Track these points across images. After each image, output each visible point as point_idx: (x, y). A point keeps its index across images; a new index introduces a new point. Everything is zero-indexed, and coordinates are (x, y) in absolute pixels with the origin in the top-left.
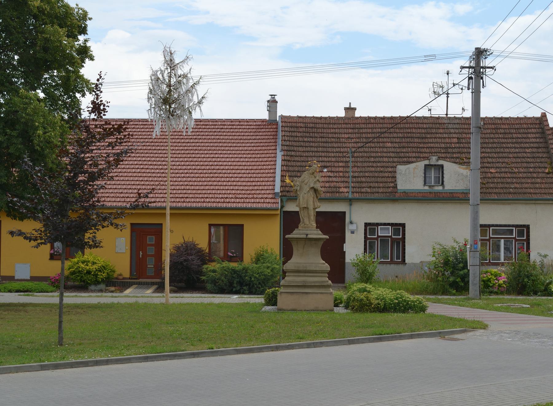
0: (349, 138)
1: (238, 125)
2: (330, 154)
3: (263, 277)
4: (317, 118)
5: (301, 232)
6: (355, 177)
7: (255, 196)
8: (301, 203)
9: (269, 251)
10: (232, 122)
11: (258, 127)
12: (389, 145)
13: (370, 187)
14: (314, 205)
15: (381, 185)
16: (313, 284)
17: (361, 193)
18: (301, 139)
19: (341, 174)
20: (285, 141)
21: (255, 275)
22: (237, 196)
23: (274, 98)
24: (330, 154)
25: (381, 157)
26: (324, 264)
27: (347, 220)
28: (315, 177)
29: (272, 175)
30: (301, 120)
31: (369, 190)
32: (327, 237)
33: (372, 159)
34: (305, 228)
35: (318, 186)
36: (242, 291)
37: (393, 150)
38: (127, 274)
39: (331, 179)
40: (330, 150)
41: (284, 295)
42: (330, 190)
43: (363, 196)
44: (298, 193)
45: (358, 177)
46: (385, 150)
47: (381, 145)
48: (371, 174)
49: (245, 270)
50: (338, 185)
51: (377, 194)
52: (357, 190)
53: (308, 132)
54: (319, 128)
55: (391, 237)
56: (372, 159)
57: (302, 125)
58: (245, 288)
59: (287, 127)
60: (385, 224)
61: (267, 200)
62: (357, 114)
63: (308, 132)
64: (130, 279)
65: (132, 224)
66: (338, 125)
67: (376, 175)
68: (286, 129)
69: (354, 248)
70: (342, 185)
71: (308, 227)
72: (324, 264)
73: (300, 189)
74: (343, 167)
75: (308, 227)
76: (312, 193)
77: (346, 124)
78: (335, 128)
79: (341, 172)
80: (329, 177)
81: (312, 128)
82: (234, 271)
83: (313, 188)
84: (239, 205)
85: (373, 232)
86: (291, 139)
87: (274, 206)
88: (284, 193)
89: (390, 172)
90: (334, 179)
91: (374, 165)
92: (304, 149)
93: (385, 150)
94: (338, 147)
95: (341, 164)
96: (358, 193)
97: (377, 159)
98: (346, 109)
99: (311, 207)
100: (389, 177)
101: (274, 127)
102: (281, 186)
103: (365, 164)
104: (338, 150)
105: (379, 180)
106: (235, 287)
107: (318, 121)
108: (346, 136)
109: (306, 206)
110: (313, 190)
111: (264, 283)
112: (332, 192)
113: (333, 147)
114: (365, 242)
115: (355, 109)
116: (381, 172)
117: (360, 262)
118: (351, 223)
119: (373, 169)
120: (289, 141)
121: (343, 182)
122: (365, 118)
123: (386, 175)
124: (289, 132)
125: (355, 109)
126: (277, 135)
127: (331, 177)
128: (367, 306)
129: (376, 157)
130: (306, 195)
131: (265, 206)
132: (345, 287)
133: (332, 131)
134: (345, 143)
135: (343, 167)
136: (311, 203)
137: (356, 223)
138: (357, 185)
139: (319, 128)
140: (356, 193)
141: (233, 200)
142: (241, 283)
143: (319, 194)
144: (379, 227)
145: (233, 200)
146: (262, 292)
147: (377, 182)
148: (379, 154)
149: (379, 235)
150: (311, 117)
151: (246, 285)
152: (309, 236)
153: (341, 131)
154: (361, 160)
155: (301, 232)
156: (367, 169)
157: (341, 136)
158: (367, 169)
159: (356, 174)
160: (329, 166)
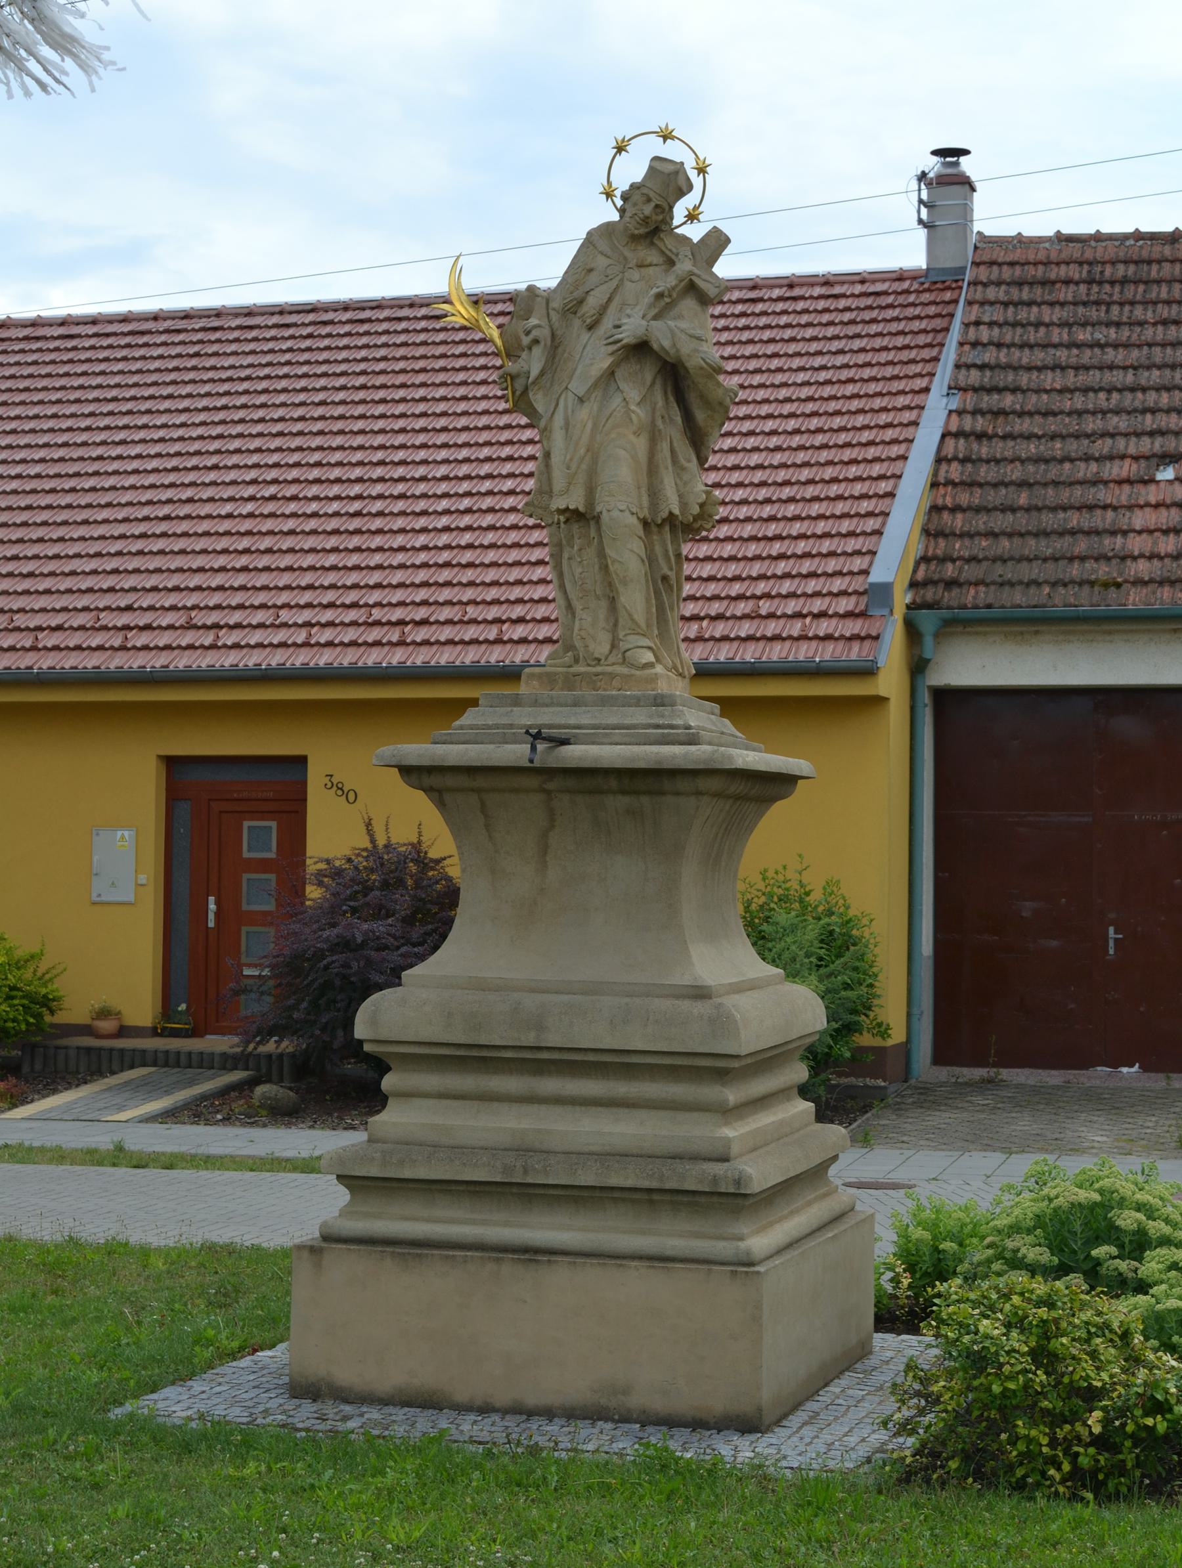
4: (1153, 237)
11: (869, 301)
16: (586, 1177)
18: (1056, 335)
20: (975, 344)
23: (957, 164)
28: (671, 263)
30: (1074, 251)
34: (570, 682)
38: (141, 1007)
53: (1097, 303)
54: (1158, 282)
57: (1074, 272)
59: (998, 284)
63: (1097, 303)
64: (154, 1032)
65: (172, 763)
68: (991, 293)
71: (592, 680)
75: (592, 680)
76: (636, 395)
81: (1124, 281)
83: (641, 349)
86: (1008, 339)
88: (930, 594)
92: (1071, 379)
107: (1157, 251)
109: (575, 501)
120: (999, 345)
124: (1006, 304)
128: (1036, 1415)
130: (584, 413)
131: (803, 652)
139: (1158, 282)
150: (1125, 237)
152: (576, 754)
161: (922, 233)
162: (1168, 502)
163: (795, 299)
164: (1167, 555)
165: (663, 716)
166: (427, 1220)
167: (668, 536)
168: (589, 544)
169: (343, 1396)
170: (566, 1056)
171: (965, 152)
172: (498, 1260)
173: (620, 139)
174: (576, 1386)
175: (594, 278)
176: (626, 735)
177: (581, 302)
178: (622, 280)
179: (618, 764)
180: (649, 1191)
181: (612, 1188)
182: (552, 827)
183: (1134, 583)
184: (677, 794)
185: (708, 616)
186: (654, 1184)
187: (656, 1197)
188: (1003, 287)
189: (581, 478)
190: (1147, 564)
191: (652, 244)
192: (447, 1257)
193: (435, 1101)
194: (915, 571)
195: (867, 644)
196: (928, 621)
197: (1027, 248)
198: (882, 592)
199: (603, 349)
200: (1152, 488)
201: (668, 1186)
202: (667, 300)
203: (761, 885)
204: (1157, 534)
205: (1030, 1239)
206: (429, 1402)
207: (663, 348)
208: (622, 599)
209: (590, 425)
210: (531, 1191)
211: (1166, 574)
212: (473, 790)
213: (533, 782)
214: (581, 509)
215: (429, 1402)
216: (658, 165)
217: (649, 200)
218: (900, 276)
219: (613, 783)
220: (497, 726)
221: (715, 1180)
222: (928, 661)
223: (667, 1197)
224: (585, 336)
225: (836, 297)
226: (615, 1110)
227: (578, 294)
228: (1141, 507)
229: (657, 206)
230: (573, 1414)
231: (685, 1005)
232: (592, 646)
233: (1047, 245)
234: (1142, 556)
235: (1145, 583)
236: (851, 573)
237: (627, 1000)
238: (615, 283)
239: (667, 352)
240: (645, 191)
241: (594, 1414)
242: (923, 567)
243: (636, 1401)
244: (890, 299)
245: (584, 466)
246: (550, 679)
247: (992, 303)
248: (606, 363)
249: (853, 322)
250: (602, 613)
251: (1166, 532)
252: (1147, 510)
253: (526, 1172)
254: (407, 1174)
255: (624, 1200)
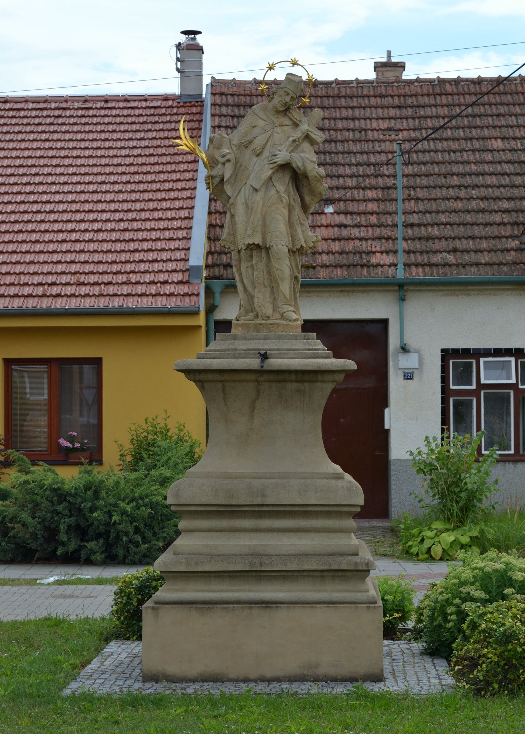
0: (389, 129)
1: (101, 108)
2: (341, 170)
3: (145, 511)
5: (240, 345)
6: (412, 225)
7: (133, 278)
8: (240, 228)
9: (173, 432)
10: (86, 101)
11: (152, 111)
12: (499, 144)
13: (455, 250)
14: (293, 237)
15: (484, 244)
17: (431, 265)
19: (373, 219)
21: (122, 504)
22: (82, 278)
23: (194, 39)
24: (341, 170)
25: (477, 174)
26: (339, 477)
27: (393, 342)
28: (296, 125)
29: (185, 224)
31: (451, 258)
32: (351, 365)
33: (455, 180)
34: (257, 328)
35: (307, 159)
36: (83, 554)
37: (509, 156)
39: (345, 232)
40: (340, 158)
41: (168, 616)
42: (343, 259)
43: (436, 275)
44: (228, 189)
45: (419, 225)
46: (488, 157)
47: (477, 144)
48: (454, 218)
49: (94, 489)
50: (365, 246)
51: (474, 269)
52: (420, 258)
55: (514, 387)
56: (455, 180)
58: (91, 545)
59: (227, 105)
60: (498, 352)
61: (168, 289)
62: (408, 75)
66: (360, 100)
67: (469, 218)
68: (224, 110)
69: (412, 423)
70: (376, 246)
71: (269, 327)
72: (339, 477)
73: (235, 174)
74: (377, 200)
76: (283, 186)
77: (381, 96)
78: (353, 108)
79: (372, 214)
80: (341, 226)
82: (60, 494)
84: (88, 303)
85: (464, 374)
87: (187, 303)
88: (216, 271)
89: (507, 211)
90: (355, 232)
91: (462, 193)
93: (488, 157)
94: (362, 153)
95: (371, 194)
96: (423, 266)
97: (468, 180)
98: (378, 67)
99: (281, 244)
100: (505, 224)
101: (194, 110)
102: (209, 253)
103: (438, 193)
104: (361, 158)
105: (477, 231)
106: (63, 544)
108: (384, 125)
109: (258, 240)
110: (287, 178)
111: (151, 527)
112: (349, 266)
113: (349, 153)
114: (444, 402)
115: (401, 66)
116: (483, 211)
117: (438, 459)
118: (404, 349)
119: (459, 205)
121: (380, 238)
122: (430, 81)
123: (497, 218)
124: (233, 117)
125: (401, 66)
126: (200, 129)
127: (346, 226)
129: (464, 175)
130: (258, 197)
131: (160, 303)
132: (393, 531)
133: (345, 113)
134: (379, 141)
135: (377, 200)
136: (280, 226)
137: (418, 351)
138: (418, 245)
140: (417, 265)
141: (69, 290)
142: (82, 531)
143: (312, 192)
144: (482, 360)
145: (69, 290)
146: (145, 556)
147: (473, 238)
148: (474, 167)
149: (483, 381)
151: (98, 536)
152: (275, 363)
153: (368, 112)
154: (425, 181)
155: (240, 345)
156: (443, 205)
157: (368, 124)
158: (443, 205)
159: (415, 219)
160: (339, 200)
161: (178, 75)
162: (333, 224)
163: (87, 109)
164: (337, 252)
165: (310, 344)
166: (208, 591)
167: (298, 257)
168: (261, 261)
169: (171, 679)
170: (275, 509)
171: (199, 33)
172: (250, 608)
173: (271, 63)
174: (292, 666)
175: (257, 131)
176: (296, 354)
177: (251, 142)
178: (272, 132)
179: (293, 368)
180: (322, 571)
181: (304, 571)
182: (257, 398)
183: (322, 267)
184: (324, 382)
185: (103, 283)
186: (326, 568)
187: (325, 574)
188: (230, 107)
189: (259, 229)
190: (327, 256)
191: (285, 115)
192: (224, 608)
193: (207, 533)
194: (207, 259)
195: (193, 298)
196: (217, 286)
197: (240, 87)
198: (194, 271)
199: (267, 166)
200: (323, 216)
201: (333, 568)
202: (297, 143)
203: (145, 426)
204: (329, 241)
205: (473, 587)
206: (216, 679)
207: (298, 166)
208: (281, 287)
209: (261, 203)
210: (262, 574)
211: (337, 262)
212: (220, 381)
213: (253, 377)
214: (261, 244)
215: (216, 679)
216: (289, 77)
217: (288, 94)
218: (166, 98)
219: (293, 377)
220: (228, 350)
221: (356, 564)
222: (217, 306)
223: (331, 574)
224: (255, 159)
225: (110, 108)
226: (299, 534)
227: (250, 138)
228: (319, 227)
229: (292, 97)
230: (292, 679)
231: (333, 482)
232: (264, 310)
233: (249, 85)
234: (323, 252)
235: (327, 267)
236: (176, 260)
237: (303, 481)
238: (269, 134)
239: (300, 169)
240: (286, 90)
241: (302, 679)
242: (210, 257)
243: (321, 671)
244: (163, 111)
245: (260, 223)
246: (247, 327)
247: (225, 116)
248: (269, 173)
249: (145, 123)
250: (268, 294)
251: (334, 240)
252: (323, 228)
253: (261, 565)
254: (200, 569)
255: (309, 576)
